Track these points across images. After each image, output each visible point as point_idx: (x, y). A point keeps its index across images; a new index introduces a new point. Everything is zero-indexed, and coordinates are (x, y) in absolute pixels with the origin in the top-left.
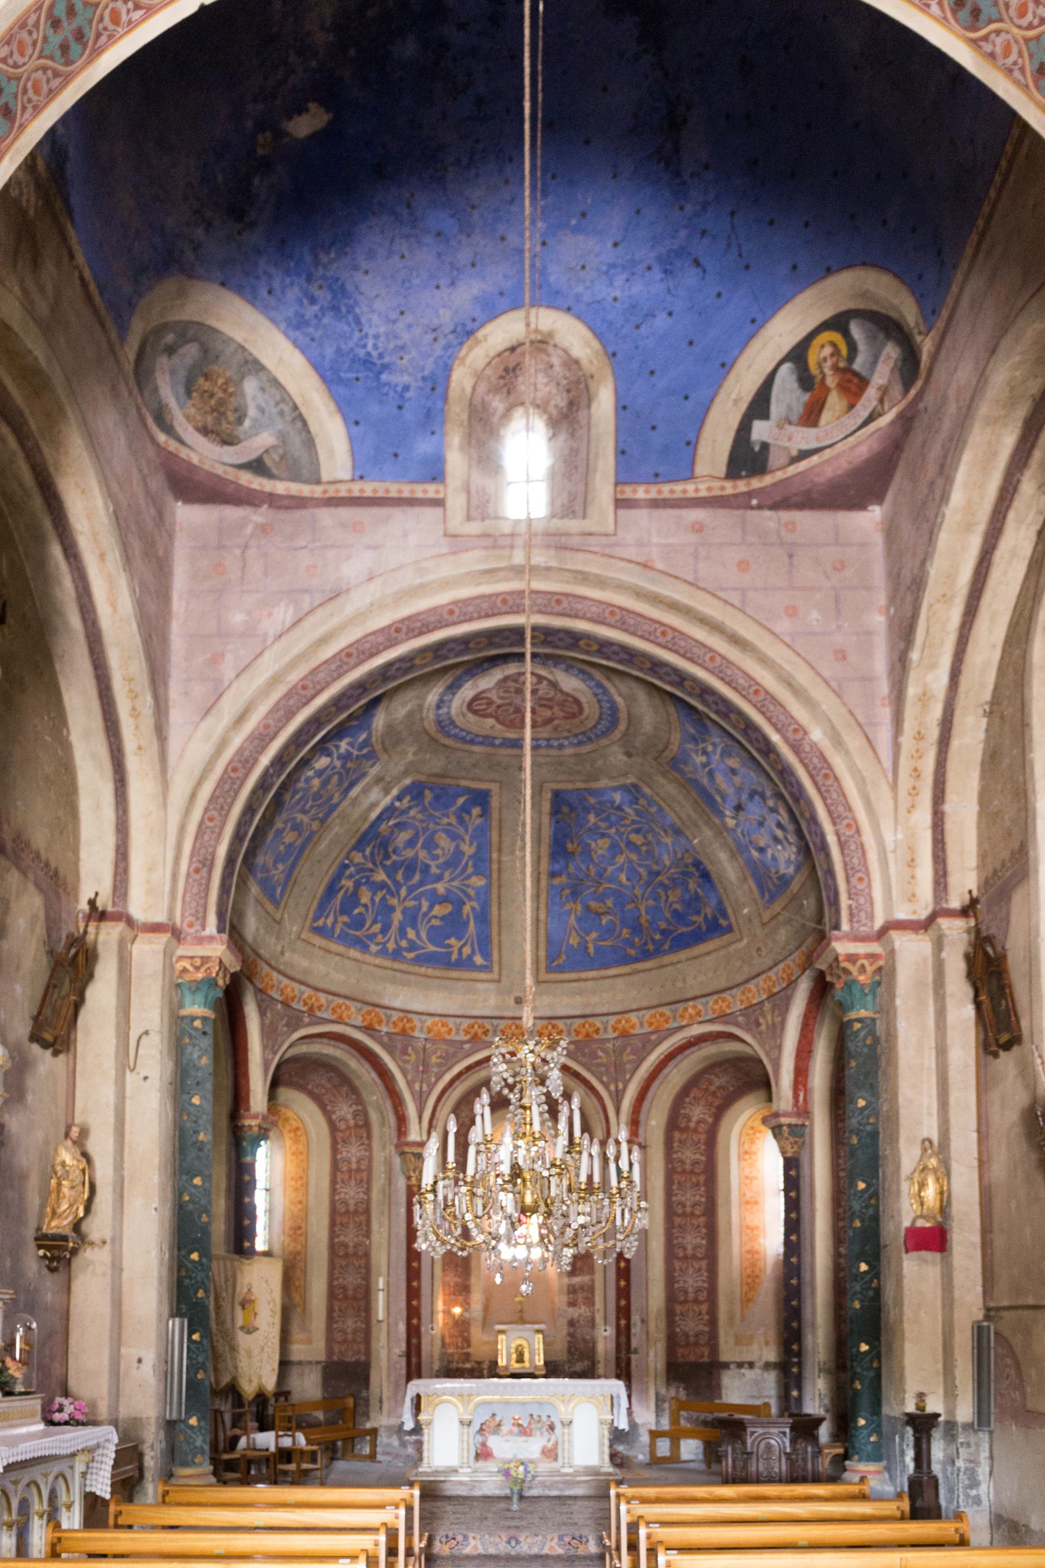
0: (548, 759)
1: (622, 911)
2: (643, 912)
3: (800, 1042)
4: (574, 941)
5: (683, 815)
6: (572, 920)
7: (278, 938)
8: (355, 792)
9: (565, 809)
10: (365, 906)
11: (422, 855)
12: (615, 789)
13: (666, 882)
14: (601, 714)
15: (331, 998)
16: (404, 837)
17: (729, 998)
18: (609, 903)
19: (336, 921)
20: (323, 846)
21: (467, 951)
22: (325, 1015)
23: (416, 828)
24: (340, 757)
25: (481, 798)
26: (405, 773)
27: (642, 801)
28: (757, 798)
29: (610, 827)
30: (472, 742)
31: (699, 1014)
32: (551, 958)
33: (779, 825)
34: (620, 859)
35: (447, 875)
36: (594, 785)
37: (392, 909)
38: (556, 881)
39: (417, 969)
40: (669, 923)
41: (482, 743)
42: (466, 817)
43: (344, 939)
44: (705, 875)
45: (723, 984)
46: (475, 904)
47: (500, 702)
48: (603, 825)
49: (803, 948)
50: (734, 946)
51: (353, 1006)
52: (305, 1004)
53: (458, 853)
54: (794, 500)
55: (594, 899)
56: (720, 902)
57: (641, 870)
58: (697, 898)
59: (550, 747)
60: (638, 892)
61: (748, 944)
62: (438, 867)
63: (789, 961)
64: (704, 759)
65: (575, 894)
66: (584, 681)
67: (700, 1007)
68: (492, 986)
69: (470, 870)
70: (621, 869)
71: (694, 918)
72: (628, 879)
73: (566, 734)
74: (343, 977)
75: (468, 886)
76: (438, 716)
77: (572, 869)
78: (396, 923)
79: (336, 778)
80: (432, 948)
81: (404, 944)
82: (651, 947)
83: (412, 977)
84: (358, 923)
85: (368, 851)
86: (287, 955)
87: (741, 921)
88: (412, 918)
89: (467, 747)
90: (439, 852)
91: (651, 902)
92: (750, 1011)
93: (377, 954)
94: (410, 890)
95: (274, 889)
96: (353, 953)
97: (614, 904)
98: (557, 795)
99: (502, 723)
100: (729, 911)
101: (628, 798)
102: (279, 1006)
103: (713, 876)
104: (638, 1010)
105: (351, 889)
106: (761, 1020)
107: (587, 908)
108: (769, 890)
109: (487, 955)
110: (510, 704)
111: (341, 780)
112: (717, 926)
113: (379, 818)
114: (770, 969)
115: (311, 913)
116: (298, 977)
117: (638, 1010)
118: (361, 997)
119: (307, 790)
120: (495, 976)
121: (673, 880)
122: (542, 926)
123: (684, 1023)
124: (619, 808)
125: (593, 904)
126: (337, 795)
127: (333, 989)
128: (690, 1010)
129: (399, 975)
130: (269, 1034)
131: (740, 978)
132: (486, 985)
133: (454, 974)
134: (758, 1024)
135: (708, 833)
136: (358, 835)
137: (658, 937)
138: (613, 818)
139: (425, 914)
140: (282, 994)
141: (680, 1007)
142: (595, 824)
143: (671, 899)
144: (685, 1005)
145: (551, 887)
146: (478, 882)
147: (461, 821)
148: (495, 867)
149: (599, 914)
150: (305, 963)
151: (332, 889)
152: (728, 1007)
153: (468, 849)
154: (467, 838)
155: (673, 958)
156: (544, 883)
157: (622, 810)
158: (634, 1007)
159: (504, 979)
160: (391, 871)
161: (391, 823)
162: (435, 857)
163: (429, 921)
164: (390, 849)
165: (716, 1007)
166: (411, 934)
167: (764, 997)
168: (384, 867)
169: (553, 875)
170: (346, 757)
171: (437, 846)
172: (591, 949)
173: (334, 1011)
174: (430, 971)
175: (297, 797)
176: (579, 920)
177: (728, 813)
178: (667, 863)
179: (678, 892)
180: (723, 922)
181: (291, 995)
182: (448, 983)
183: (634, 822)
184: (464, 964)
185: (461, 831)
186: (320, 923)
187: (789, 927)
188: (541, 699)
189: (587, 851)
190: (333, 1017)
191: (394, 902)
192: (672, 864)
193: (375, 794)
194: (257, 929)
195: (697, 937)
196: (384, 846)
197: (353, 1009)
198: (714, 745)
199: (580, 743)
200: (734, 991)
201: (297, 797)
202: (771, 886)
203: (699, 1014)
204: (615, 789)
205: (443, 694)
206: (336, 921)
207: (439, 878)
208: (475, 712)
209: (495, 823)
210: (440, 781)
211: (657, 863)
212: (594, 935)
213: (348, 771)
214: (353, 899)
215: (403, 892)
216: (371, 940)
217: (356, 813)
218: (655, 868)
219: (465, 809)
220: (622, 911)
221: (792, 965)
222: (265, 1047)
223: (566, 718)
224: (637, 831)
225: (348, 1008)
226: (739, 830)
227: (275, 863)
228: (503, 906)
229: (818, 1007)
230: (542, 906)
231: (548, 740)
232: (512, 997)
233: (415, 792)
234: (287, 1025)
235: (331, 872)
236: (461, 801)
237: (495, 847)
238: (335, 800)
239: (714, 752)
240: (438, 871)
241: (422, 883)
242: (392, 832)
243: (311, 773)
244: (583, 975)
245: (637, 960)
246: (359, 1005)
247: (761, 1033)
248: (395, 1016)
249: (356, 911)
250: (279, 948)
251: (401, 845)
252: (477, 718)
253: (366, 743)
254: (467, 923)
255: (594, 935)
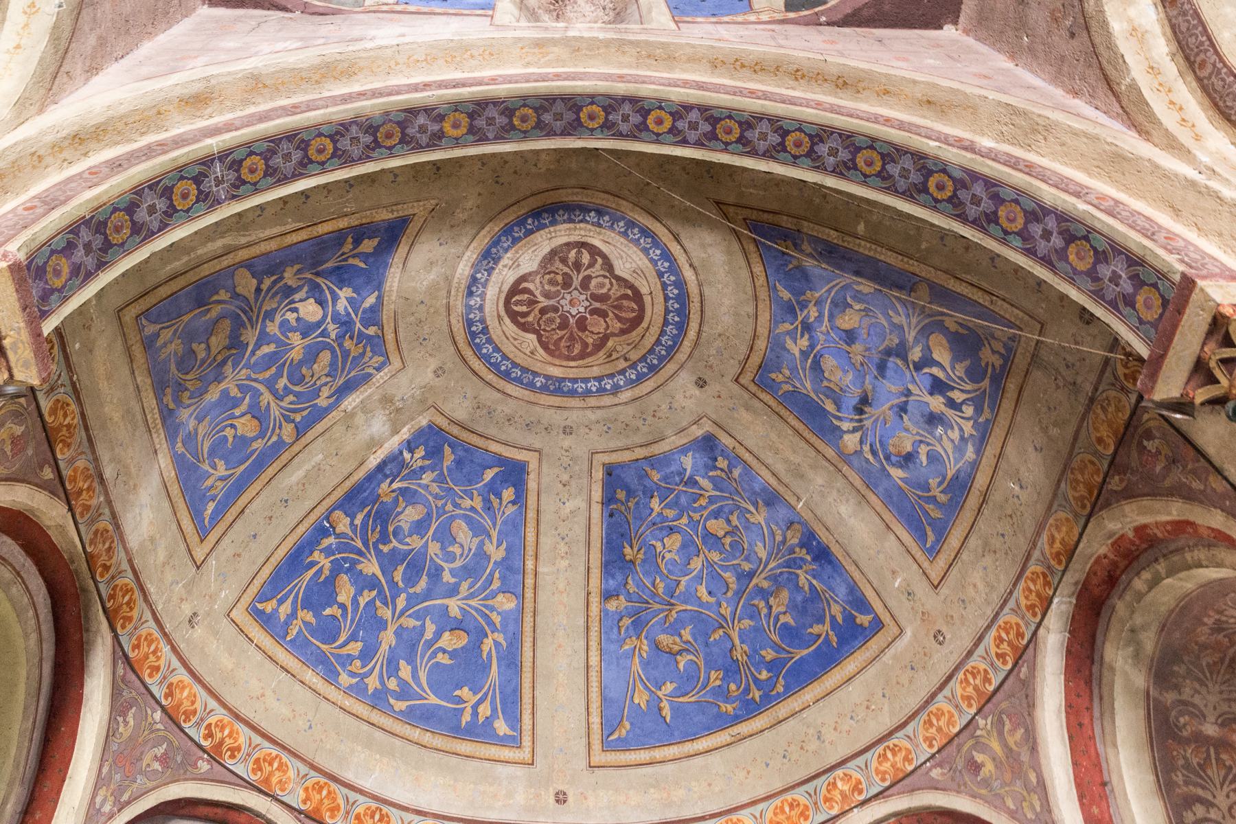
0: (599, 414)
1: (707, 645)
2: (737, 642)
3: (1075, 764)
4: (641, 698)
5: (780, 468)
6: (636, 666)
7: (189, 587)
8: (351, 401)
9: (621, 495)
10: (343, 606)
11: (434, 548)
12: (684, 450)
13: (765, 584)
14: (667, 311)
15: (257, 739)
16: (410, 515)
17: (905, 744)
18: (687, 634)
19: (293, 615)
20: (294, 476)
21: (485, 710)
22: (240, 769)
23: (429, 507)
24: (336, 318)
25: (514, 474)
26: (424, 404)
27: (722, 463)
28: (894, 362)
29: (679, 517)
30: (506, 376)
31: (857, 788)
32: (609, 726)
33: (938, 387)
34: (697, 564)
35: (465, 586)
36: (657, 449)
37: (383, 625)
38: (612, 606)
39: (407, 730)
40: (777, 648)
41: (518, 380)
42: (495, 501)
43: (299, 647)
44: (822, 555)
45: (887, 721)
46: (500, 638)
47: (544, 302)
48: (670, 513)
49: (1033, 567)
50: (891, 652)
51: (295, 768)
52: (209, 735)
53: (481, 555)
54: (865, 13)
55: (664, 631)
56: (853, 589)
57: (727, 575)
58: (815, 594)
59: (601, 391)
60: (726, 610)
61: (914, 636)
62: (451, 571)
63: (1007, 617)
64: (804, 342)
65: (638, 625)
66: (645, 251)
67: (856, 775)
68: (519, 771)
69: (496, 584)
70: (699, 578)
71: (816, 629)
72: (710, 593)
73: (622, 364)
74: (286, 711)
75: (492, 609)
76: (469, 309)
77: (632, 587)
78: (384, 647)
79: (325, 357)
80: (433, 700)
81: (392, 684)
82: (757, 694)
83: (397, 742)
84: (329, 632)
85: (358, 521)
86: (199, 631)
87: (892, 603)
88: (409, 645)
89: (501, 384)
90: (456, 549)
91: (747, 623)
92: (952, 749)
93: (348, 691)
94: (413, 600)
95: (203, 498)
96: (310, 676)
97: (693, 635)
98: (610, 471)
99: (545, 347)
100: (870, 595)
101: (702, 459)
102: (158, 715)
103: (835, 549)
104: (754, 803)
105: (326, 572)
106: (979, 758)
107: (656, 646)
108: (933, 522)
109: (514, 720)
110: (556, 310)
111: (333, 364)
112: (857, 629)
113: (380, 467)
114: (970, 653)
115: (258, 583)
116: (208, 679)
117: (754, 803)
118: (309, 756)
119: (284, 346)
120: (525, 754)
121: (774, 578)
122: (594, 675)
123: (835, 812)
124: (692, 482)
125: (665, 639)
126: (325, 392)
127: (265, 726)
128: (839, 784)
129: (378, 734)
130: (118, 758)
131: (914, 702)
132: (510, 769)
133: (465, 747)
134: (976, 767)
135: (819, 480)
136: (348, 484)
137: (764, 675)
138: (683, 500)
139: (430, 644)
140: (170, 694)
141: (821, 782)
142: (660, 514)
143: (775, 611)
144: (829, 777)
145: (604, 613)
146: (506, 603)
147: (488, 507)
148: (529, 581)
149: (673, 654)
150: (227, 662)
151: (296, 561)
152: (907, 759)
153: (496, 553)
154: (494, 534)
155: (794, 703)
156: (595, 609)
157: (696, 482)
158: (745, 799)
159: (539, 760)
160: (390, 562)
161: (395, 486)
162: (451, 558)
163: (435, 654)
164: (391, 529)
165: (886, 766)
166: (405, 671)
167: (973, 711)
168: (379, 553)
169: (607, 596)
170: (345, 324)
171: (454, 540)
172: (667, 712)
173: (258, 767)
174: (427, 738)
175: (267, 349)
176: (646, 664)
177: (845, 426)
178: (763, 554)
179: (785, 595)
180: (864, 619)
181: (186, 705)
182: (454, 760)
183: (712, 500)
184: (479, 732)
185: (487, 522)
186: (269, 607)
187: (988, 560)
188: (595, 297)
189: (652, 558)
190: (253, 778)
191: (386, 613)
192: (770, 555)
193: (378, 425)
194: (152, 539)
195: (828, 659)
196: (383, 517)
197: (291, 773)
198: (818, 303)
199: (640, 378)
200: (909, 729)
201: (267, 349)
202: (936, 514)
203: (857, 788)
204: (684, 450)
205: (476, 267)
206: (293, 615)
207: (453, 591)
208: (514, 316)
209: (531, 515)
210: (465, 435)
211: (747, 559)
212: (669, 687)
213: (346, 354)
214: (322, 594)
215: (401, 602)
216: (343, 666)
217: (352, 442)
218: (747, 567)
219: (493, 489)
220: (707, 645)
221: (1014, 619)
222: (100, 782)
223: (623, 332)
224: (716, 515)
225: (282, 767)
226: (866, 448)
227: (213, 452)
228: (539, 643)
229: (1089, 682)
230: (594, 644)
231: (599, 379)
232: (552, 792)
233: (432, 440)
234: (164, 760)
235: (301, 529)
236: (489, 474)
237: (530, 551)
238: (322, 402)
239: (820, 318)
240: (453, 580)
241: (427, 595)
242: (396, 501)
243: (291, 317)
244: (658, 754)
245: (737, 719)
246: (304, 769)
247: (986, 783)
248: (363, 804)
249: (328, 611)
250: (187, 609)
251: (406, 527)
252: (515, 328)
253: (376, 309)
254: (486, 667)
255: (669, 687)
